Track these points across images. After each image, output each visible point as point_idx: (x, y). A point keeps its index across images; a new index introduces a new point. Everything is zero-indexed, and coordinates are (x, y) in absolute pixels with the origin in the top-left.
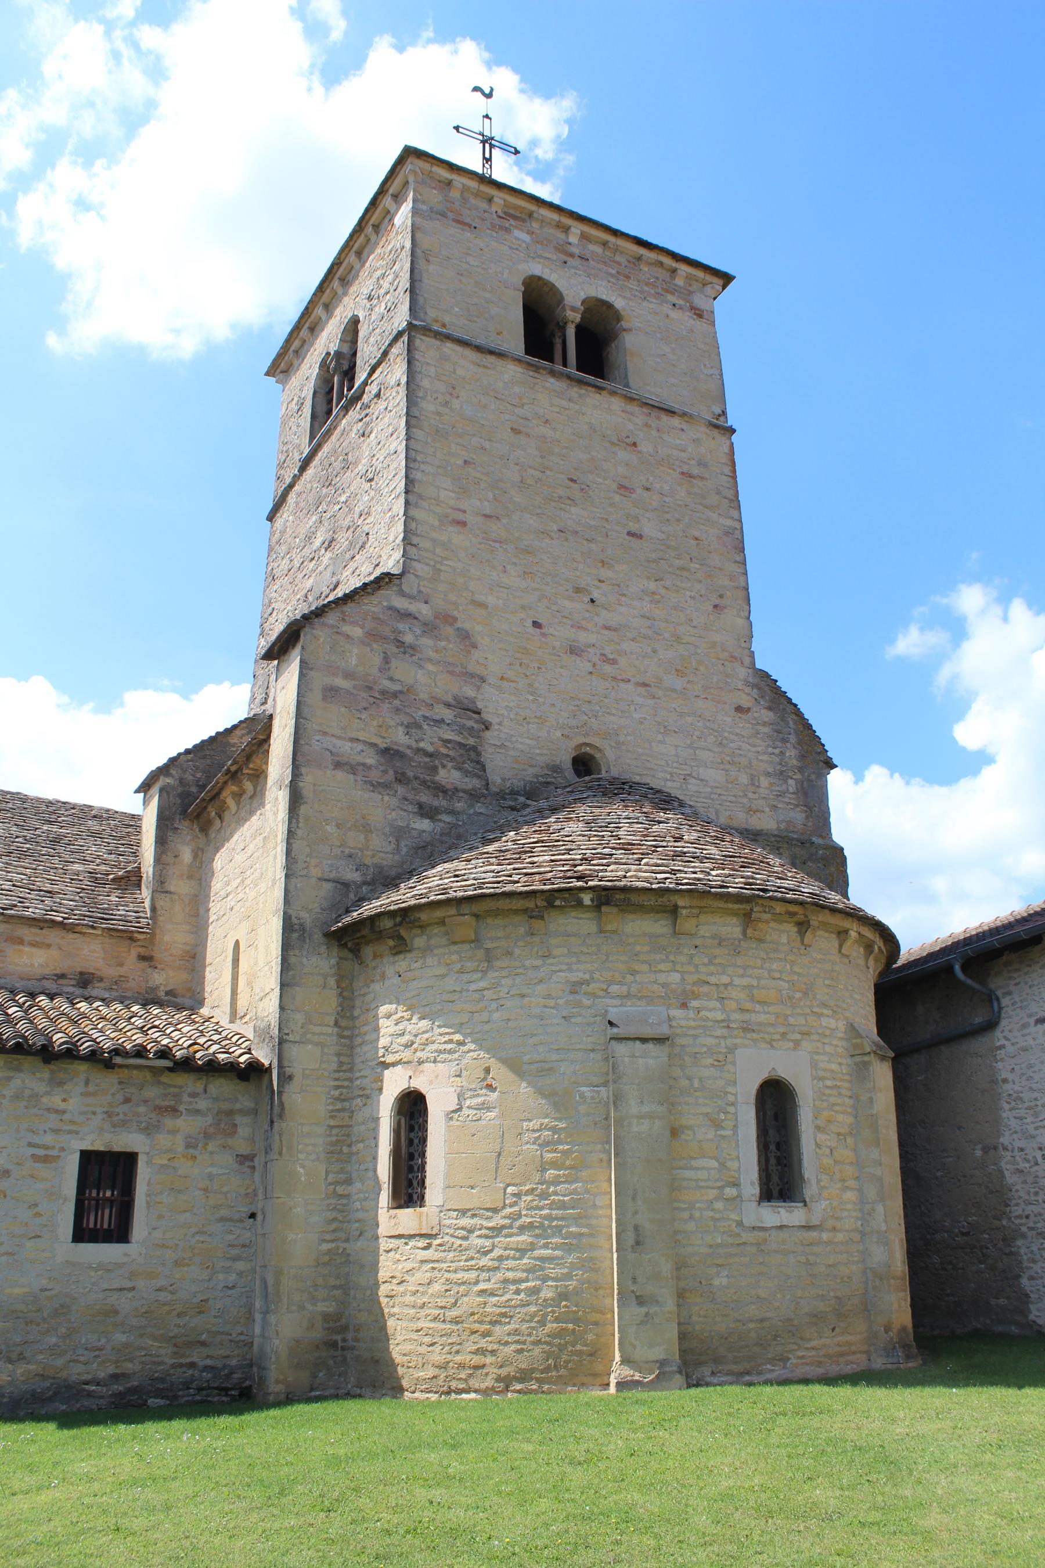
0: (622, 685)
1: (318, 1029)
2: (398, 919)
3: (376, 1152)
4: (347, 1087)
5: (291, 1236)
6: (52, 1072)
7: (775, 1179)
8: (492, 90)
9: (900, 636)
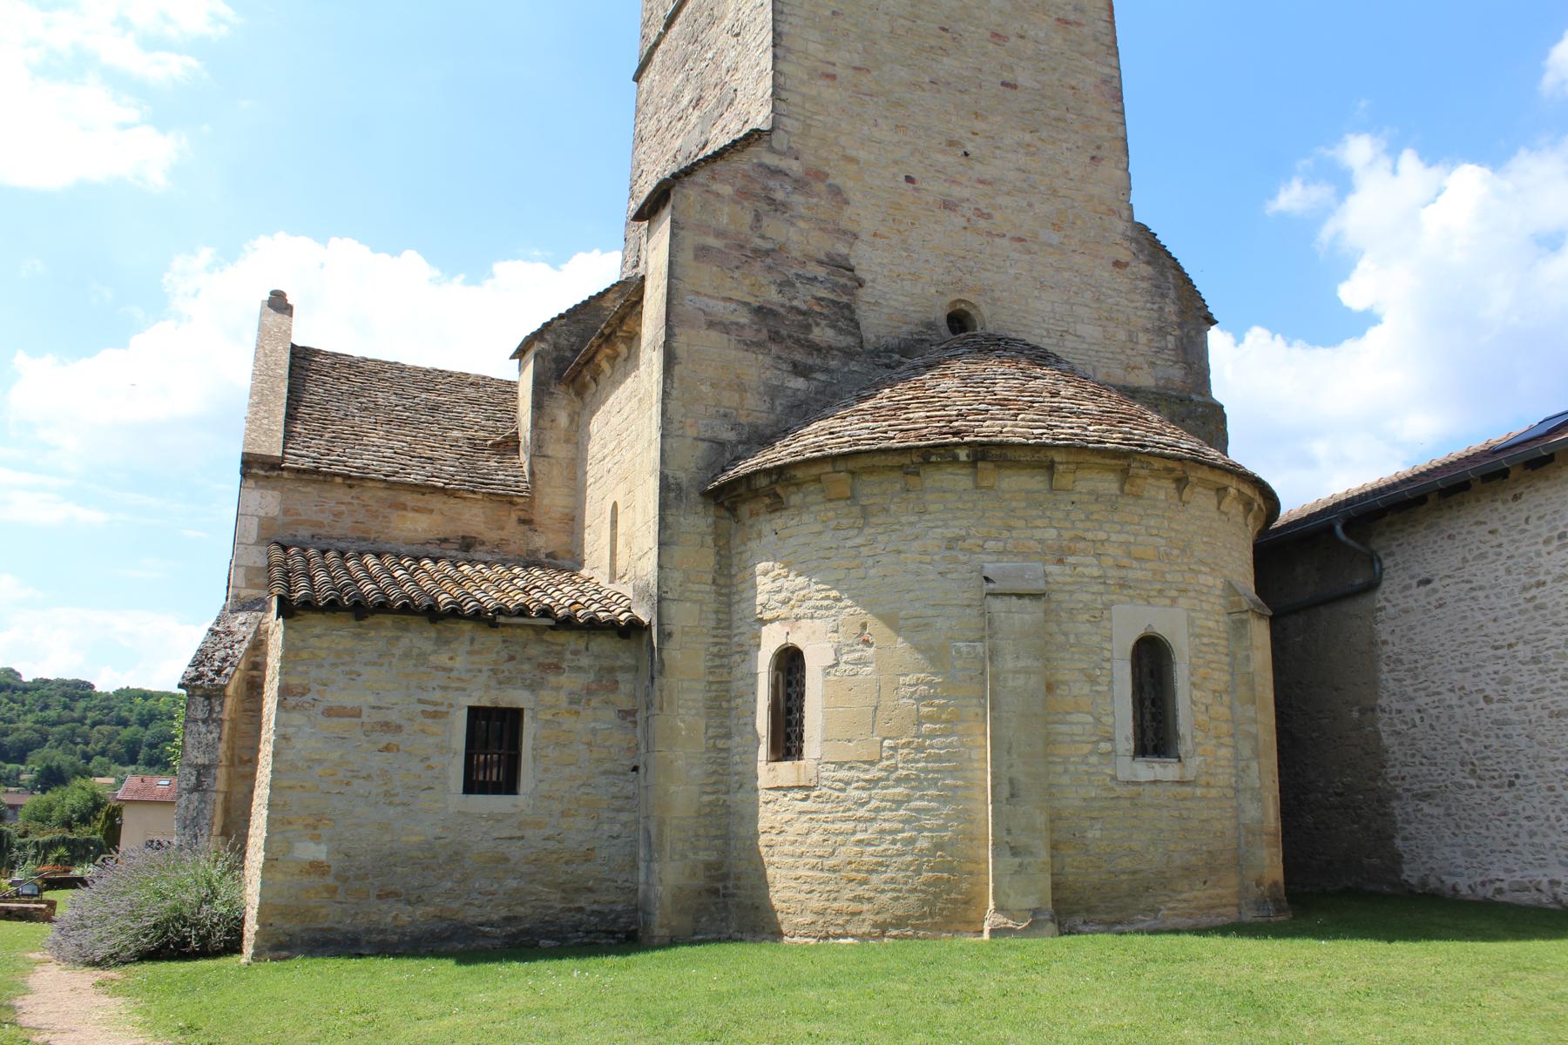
0: (997, 240)
1: (696, 587)
5: (673, 788)
6: (439, 632)
7: (1150, 734)
9: (1282, 190)
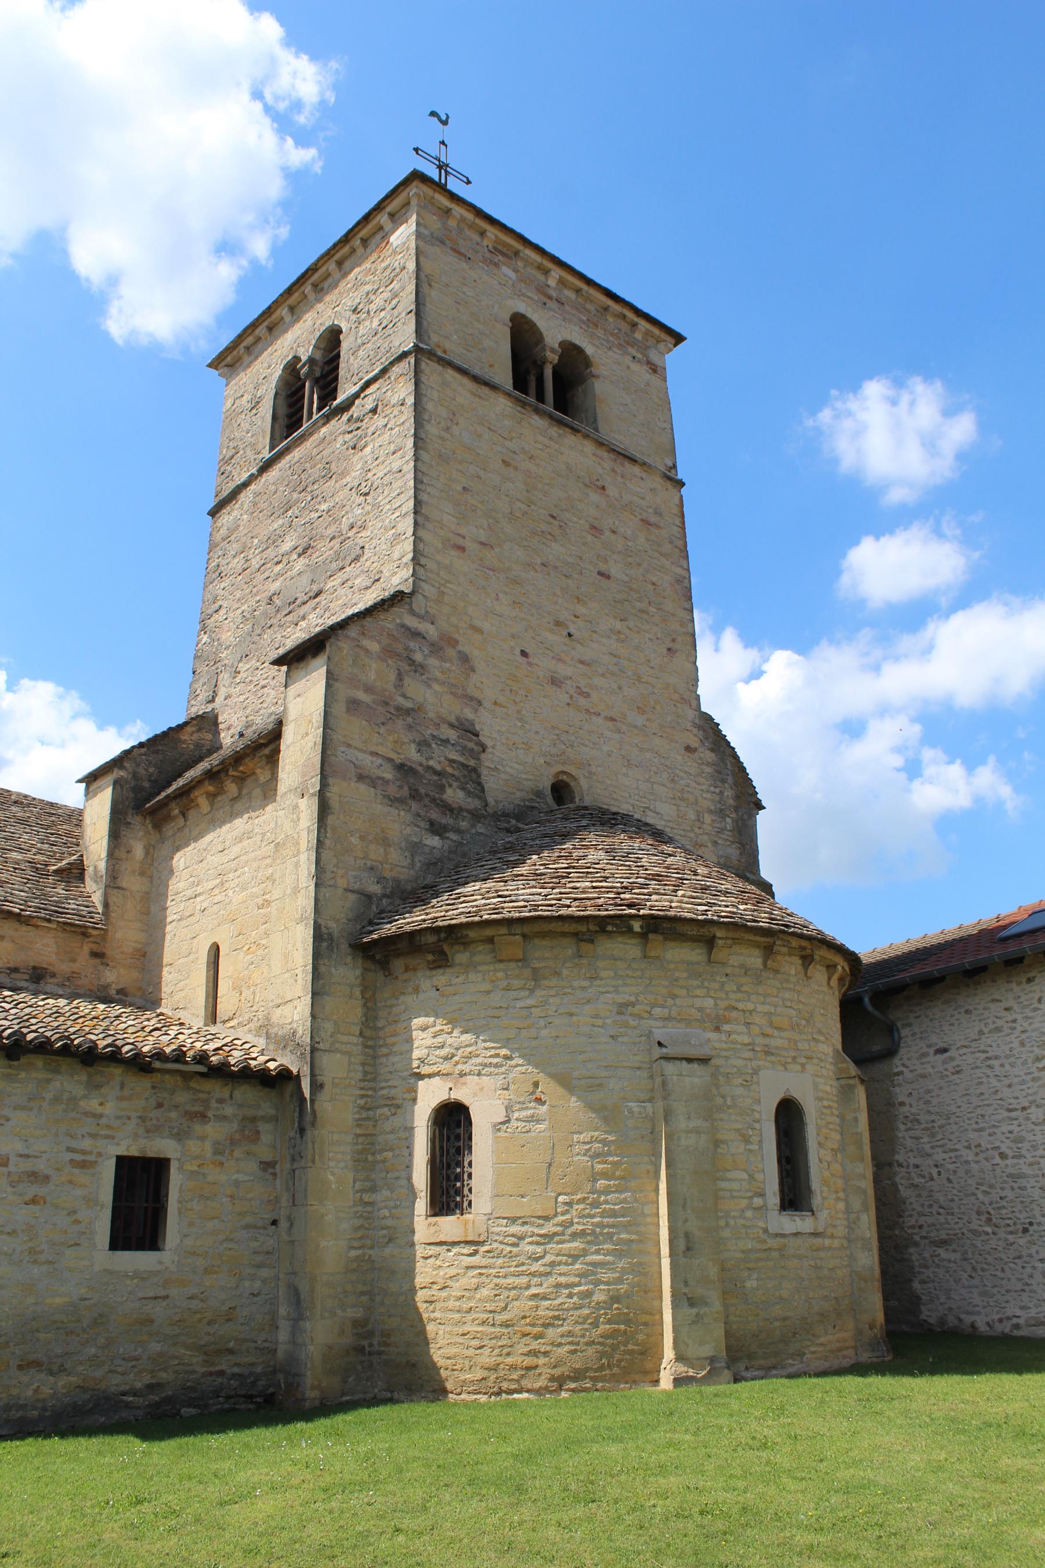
0: (594, 718)
1: (345, 1039)
2: (443, 935)
3: (411, 1161)
4: (371, 1097)
5: (323, 1244)
6: (90, 1076)
8: (448, 117)
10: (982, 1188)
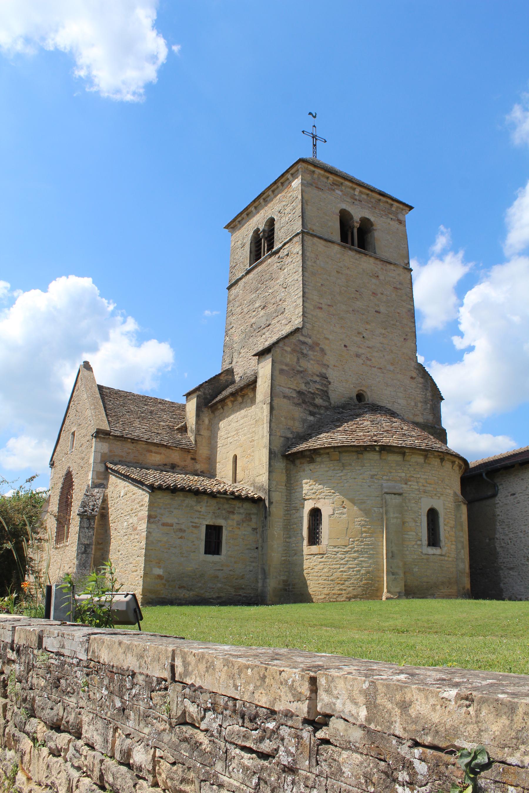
0: (373, 368)
1: (280, 487)
2: (312, 452)
5: (273, 554)
10: (526, 547)
